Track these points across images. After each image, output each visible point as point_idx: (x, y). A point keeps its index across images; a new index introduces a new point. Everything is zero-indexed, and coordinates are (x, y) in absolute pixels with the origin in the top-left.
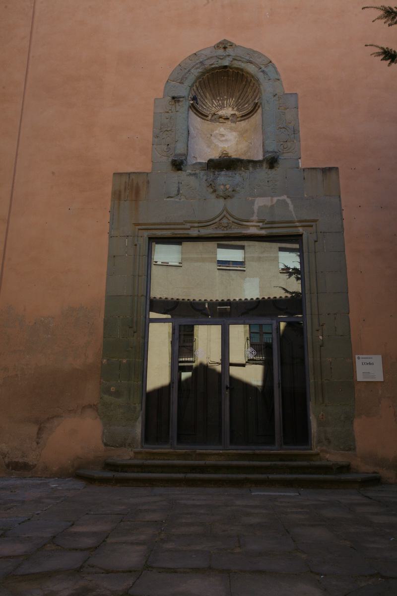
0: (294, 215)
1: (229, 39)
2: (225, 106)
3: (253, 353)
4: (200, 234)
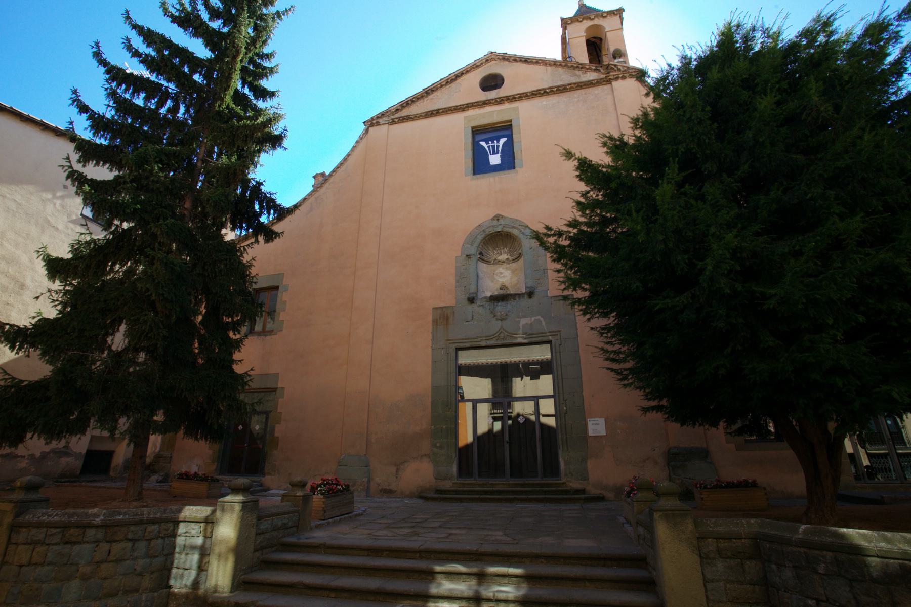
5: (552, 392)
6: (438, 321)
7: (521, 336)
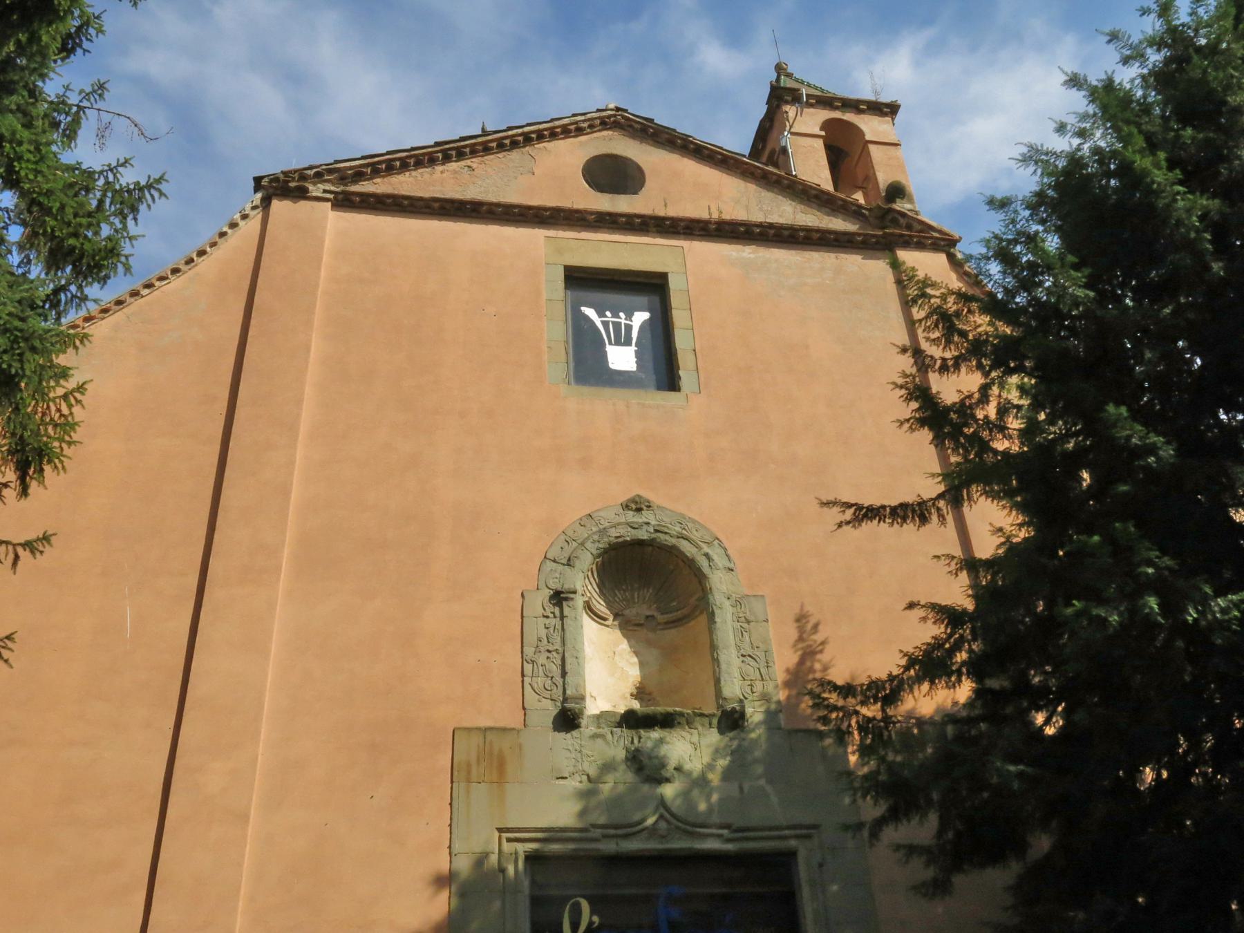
1: (647, 494)
2: (636, 600)
7: (714, 831)
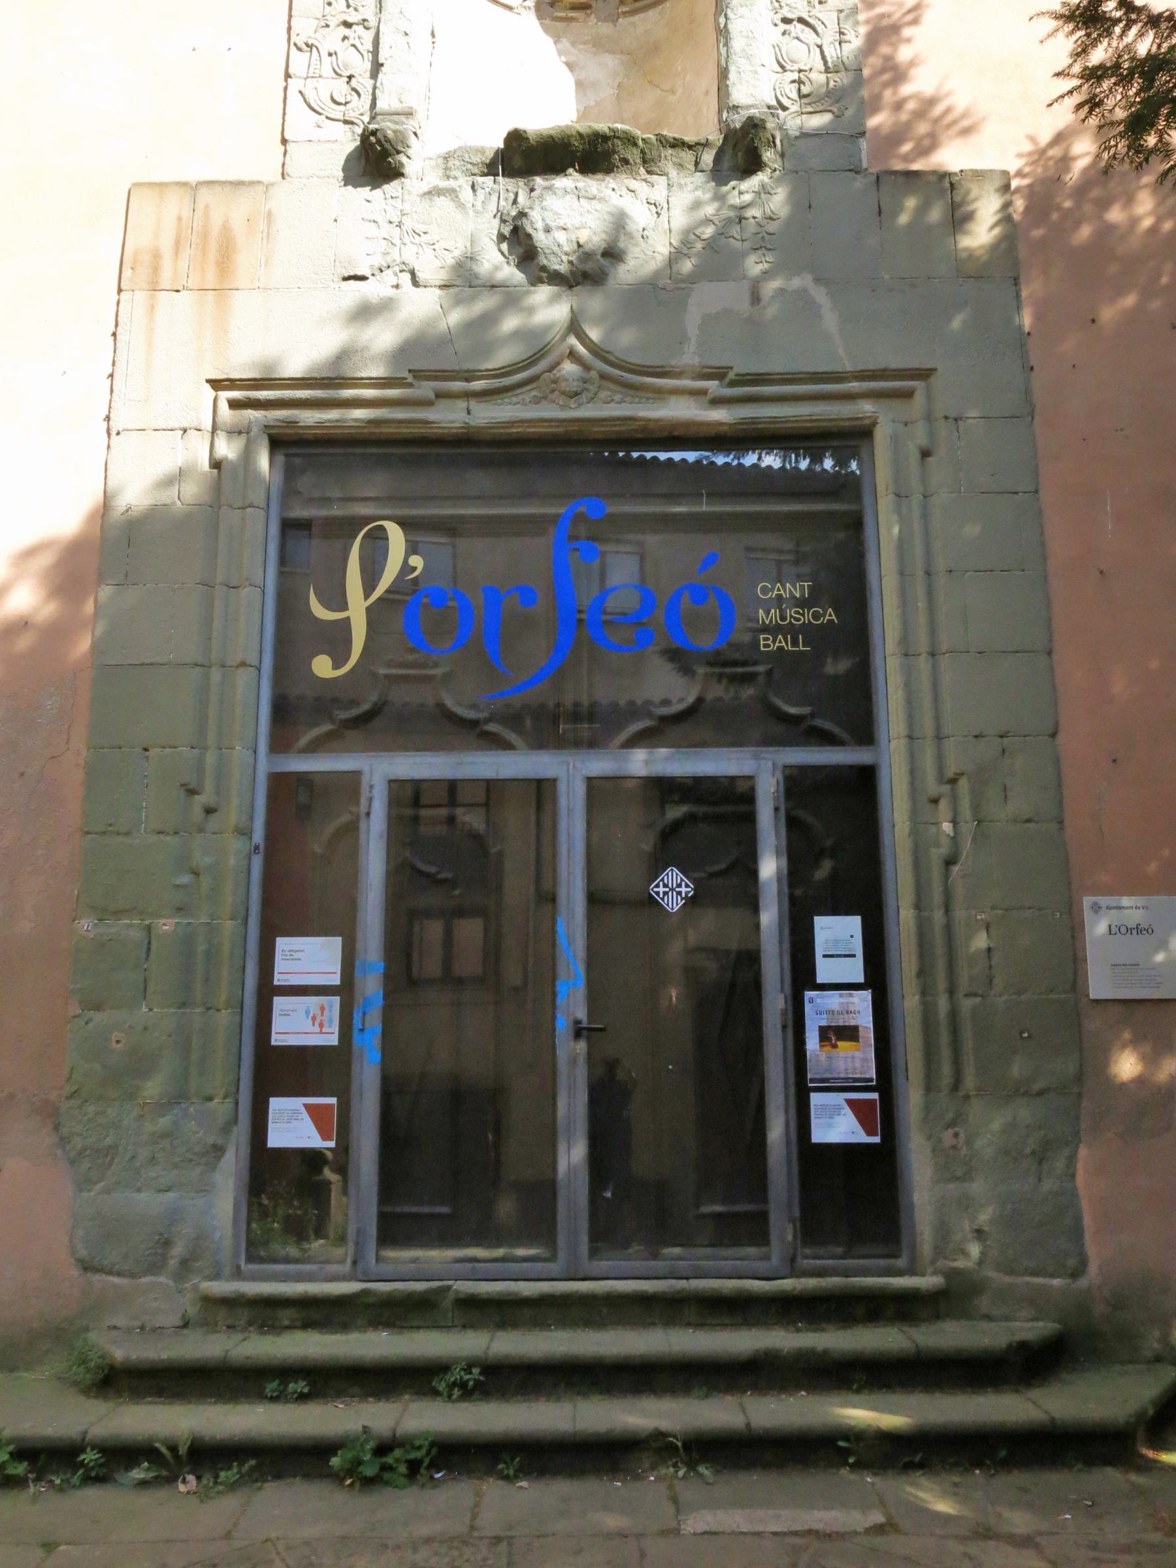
0: (841, 351)
3: (683, 890)
4: (473, 423)
5: (338, 968)
6: (167, 264)
